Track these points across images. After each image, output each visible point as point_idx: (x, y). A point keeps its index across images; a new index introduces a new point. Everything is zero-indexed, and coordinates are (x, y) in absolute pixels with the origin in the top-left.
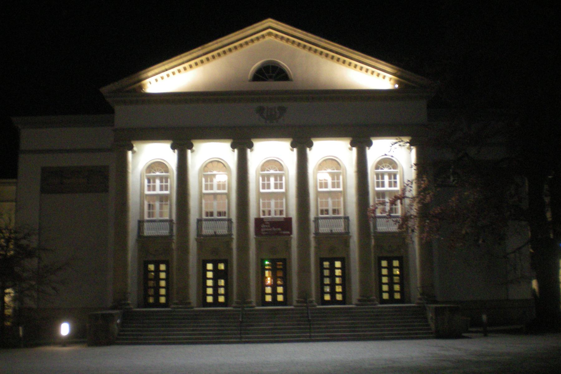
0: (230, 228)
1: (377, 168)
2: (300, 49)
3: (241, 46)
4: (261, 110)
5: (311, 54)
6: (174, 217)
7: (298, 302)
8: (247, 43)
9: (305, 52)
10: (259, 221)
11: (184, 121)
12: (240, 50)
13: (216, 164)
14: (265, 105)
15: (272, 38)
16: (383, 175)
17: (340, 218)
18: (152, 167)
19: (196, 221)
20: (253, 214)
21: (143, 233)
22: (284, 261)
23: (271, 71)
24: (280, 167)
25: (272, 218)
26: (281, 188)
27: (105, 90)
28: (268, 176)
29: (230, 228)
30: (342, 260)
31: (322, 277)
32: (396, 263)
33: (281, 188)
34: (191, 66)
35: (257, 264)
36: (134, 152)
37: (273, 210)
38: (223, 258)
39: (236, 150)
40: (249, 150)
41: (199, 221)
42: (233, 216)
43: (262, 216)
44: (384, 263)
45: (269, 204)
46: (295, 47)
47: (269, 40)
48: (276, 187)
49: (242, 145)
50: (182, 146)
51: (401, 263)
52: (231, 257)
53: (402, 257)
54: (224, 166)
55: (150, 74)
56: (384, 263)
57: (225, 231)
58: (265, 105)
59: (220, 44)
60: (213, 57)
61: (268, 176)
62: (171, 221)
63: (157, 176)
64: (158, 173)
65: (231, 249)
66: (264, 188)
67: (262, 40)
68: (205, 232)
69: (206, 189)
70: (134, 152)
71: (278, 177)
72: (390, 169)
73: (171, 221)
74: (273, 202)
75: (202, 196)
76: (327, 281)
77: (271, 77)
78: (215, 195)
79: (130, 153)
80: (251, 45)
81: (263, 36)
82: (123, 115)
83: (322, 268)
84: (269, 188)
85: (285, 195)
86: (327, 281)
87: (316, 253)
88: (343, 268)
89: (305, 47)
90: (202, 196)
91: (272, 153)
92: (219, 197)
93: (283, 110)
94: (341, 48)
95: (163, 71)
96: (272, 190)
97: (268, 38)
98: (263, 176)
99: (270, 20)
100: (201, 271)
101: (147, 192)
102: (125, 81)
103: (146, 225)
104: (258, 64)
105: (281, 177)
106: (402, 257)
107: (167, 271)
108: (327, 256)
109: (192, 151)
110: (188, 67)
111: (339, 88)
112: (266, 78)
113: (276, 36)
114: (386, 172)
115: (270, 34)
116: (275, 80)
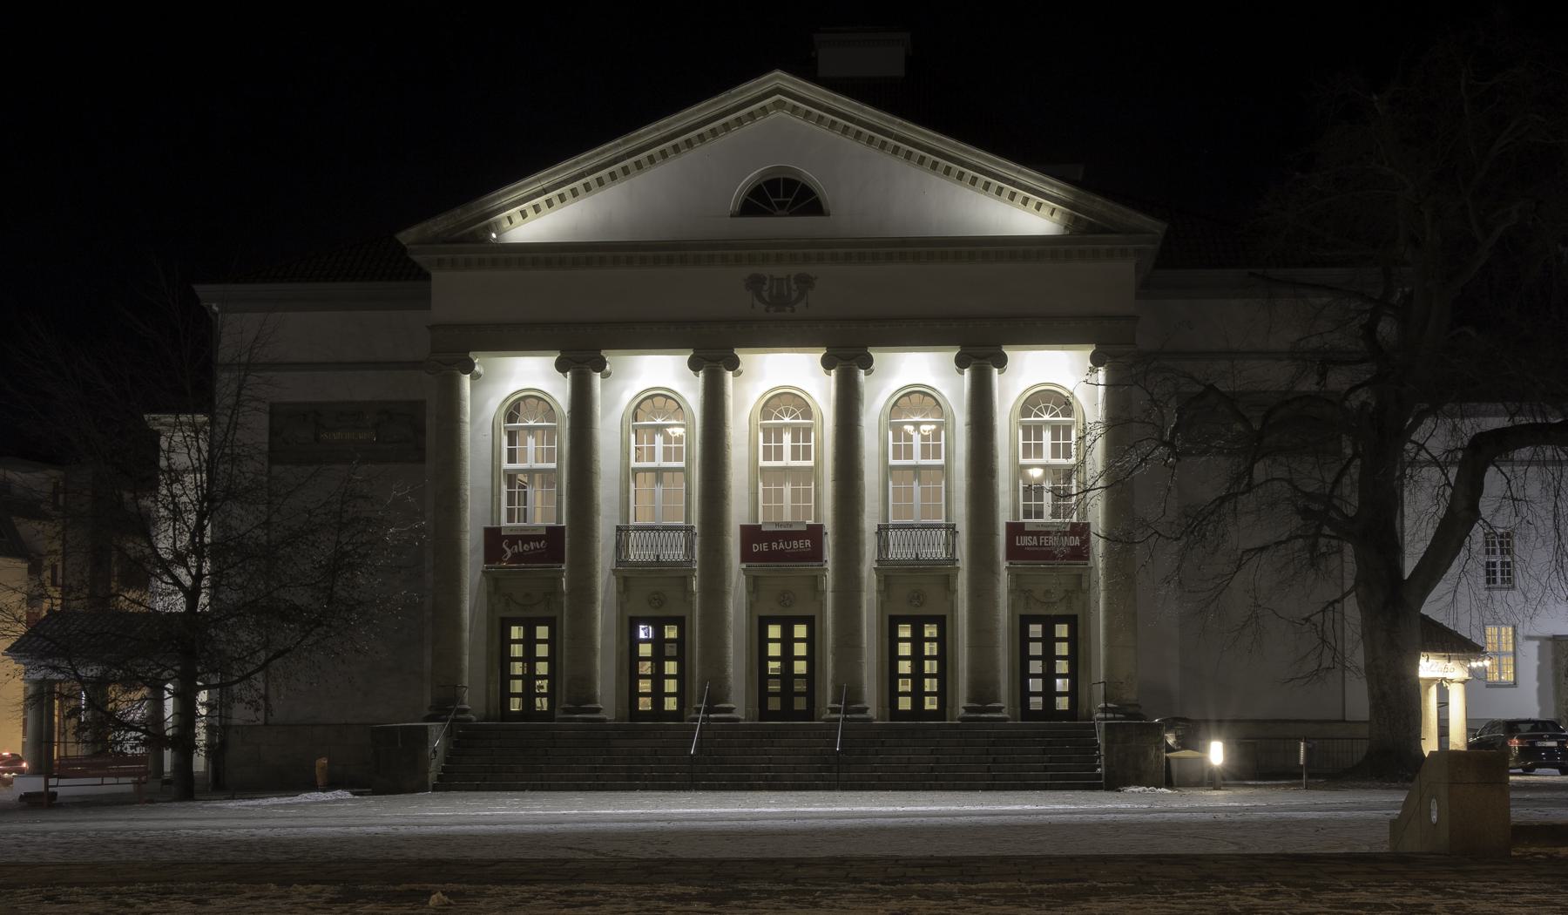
0: (951, 546)
1: (1025, 411)
2: (847, 141)
3: (714, 132)
4: (755, 283)
5: (873, 152)
6: (695, 521)
7: (968, 710)
8: (727, 127)
9: (859, 147)
10: (751, 534)
11: (586, 307)
12: (714, 144)
13: (659, 401)
14: (765, 271)
15: (783, 114)
16: (1039, 430)
17: (938, 527)
18: (513, 411)
19: (480, 535)
20: (738, 513)
21: (628, 555)
22: (941, 621)
23: (782, 194)
24: (807, 412)
25: (517, 528)
26: (807, 457)
27: (407, 237)
28: (779, 430)
29: (951, 546)
30: (1072, 621)
31: (1025, 658)
32: (542, 632)
33: (1068, 455)
34: (587, 187)
35: (1011, 631)
36: (476, 377)
37: (787, 509)
38: (675, 613)
39: (833, 372)
40: (729, 374)
41: (883, 530)
42: (961, 514)
43: (1022, 520)
44: (516, 632)
45: (780, 494)
46: (835, 136)
47: (775, 121)
48: (795, 457)
49: (714, 363)
50: (582, 363)
51: (811, 631)
52: (953, 607)
53: (1075, 617)
54: (938, 403)
55: (506, 201)
56: (774, 631)
57: (940, 553)
58: (765, 271)
59: (664, 132)
60: (639, 165)
61: (779, 430)
62: (688, 529)
63: (786, 425)
64: (787, 420)
65: (823, 592)
66: (767, 457)
67: (761, 121)
68: (893, 553)
69: (767, 457)
70: (476, 377)
71: (1061, 431)
72: (1057, 415)
73: (688, 529)
74: (787, 489)
75: (629, 475)
76: (1036, 667)
77: (781, 205)
78: (659, 473)
79: (466, 380)
80: (737, 132)
81: (764, 110)
82: (454, 293)
83: (1025, 640)
84: (779, 457)
85: (811, 474)
86: (1036, 667)
87: (1013, 606)
88: (1072, 640)
89: (858, 135)
90: (629, 475)
91: (783, 374)
92: (640, 476)
93: (805, 282)
94: (938, 140)
95: (538, 195)
96: (787, 461)
97: (774, 115)
98: (767, 431)
99: (778, 73)
100: (627, 643)
101: (762, 463)
102: (460, 214)
103: (892, 533)
104: (751, 177)
105: (807, 431)
106: (1075, 617)
107: (551, 642)
108: (778, 611)
109: (606, 376)
110: (594, 184)
111: (934, 232)
112: (769, 204)
113: (794, 110)
114: (1046, 422)
115: (779, 105)
116: (791, 215)
